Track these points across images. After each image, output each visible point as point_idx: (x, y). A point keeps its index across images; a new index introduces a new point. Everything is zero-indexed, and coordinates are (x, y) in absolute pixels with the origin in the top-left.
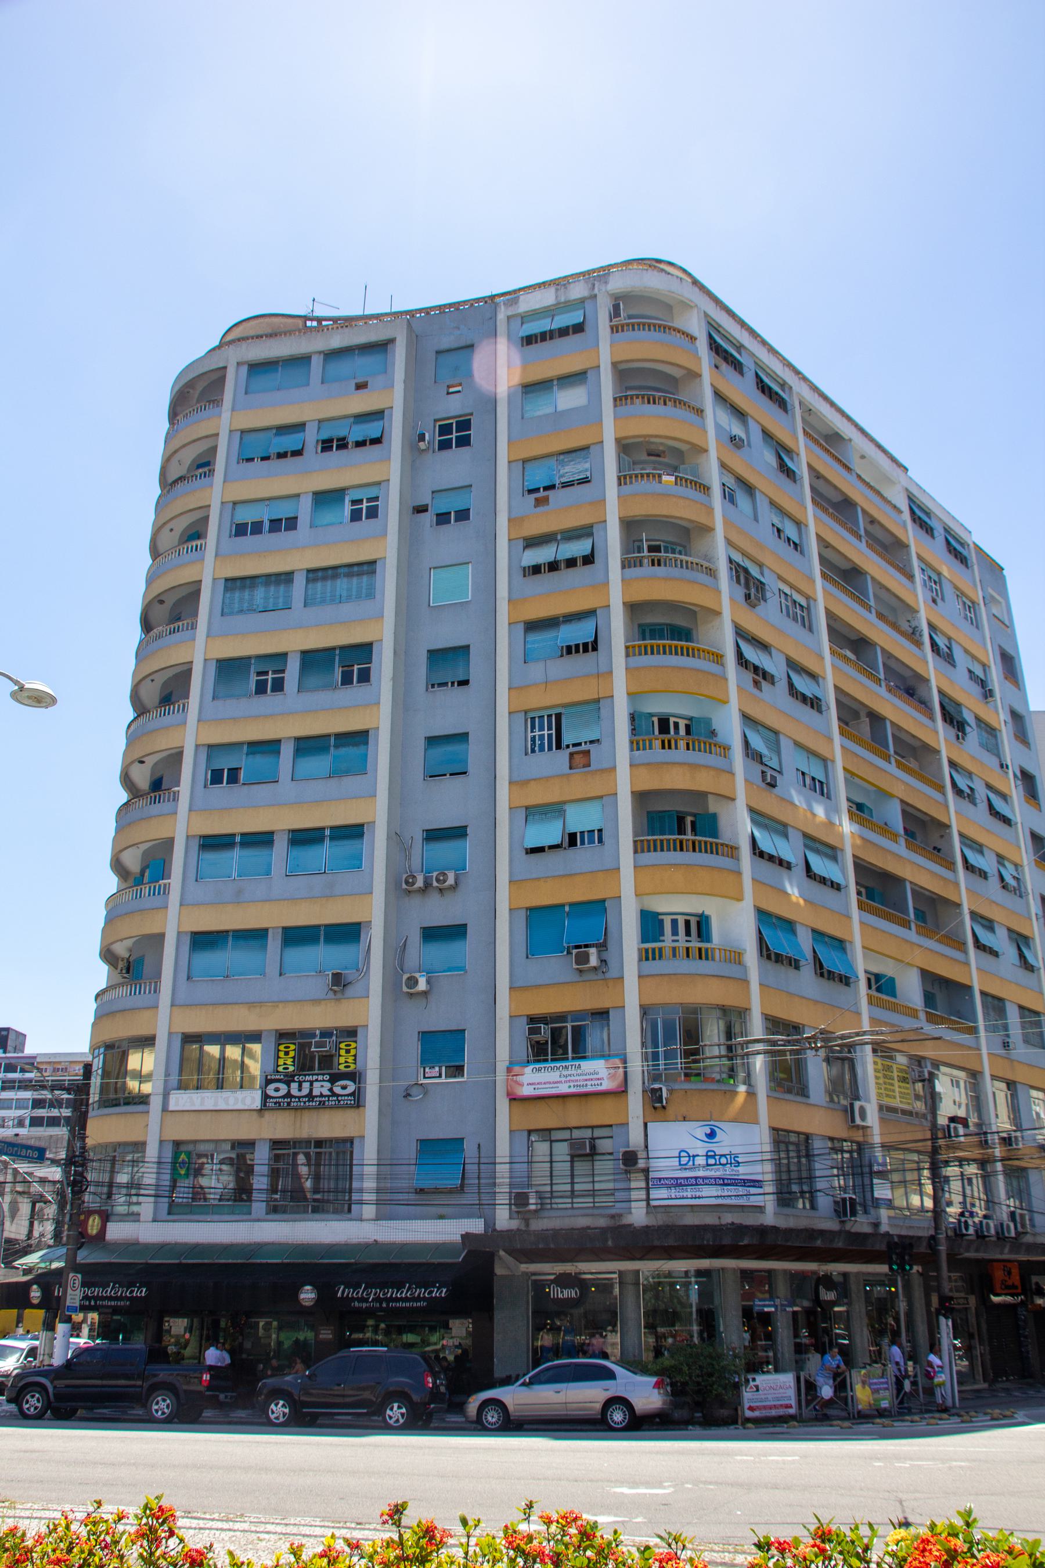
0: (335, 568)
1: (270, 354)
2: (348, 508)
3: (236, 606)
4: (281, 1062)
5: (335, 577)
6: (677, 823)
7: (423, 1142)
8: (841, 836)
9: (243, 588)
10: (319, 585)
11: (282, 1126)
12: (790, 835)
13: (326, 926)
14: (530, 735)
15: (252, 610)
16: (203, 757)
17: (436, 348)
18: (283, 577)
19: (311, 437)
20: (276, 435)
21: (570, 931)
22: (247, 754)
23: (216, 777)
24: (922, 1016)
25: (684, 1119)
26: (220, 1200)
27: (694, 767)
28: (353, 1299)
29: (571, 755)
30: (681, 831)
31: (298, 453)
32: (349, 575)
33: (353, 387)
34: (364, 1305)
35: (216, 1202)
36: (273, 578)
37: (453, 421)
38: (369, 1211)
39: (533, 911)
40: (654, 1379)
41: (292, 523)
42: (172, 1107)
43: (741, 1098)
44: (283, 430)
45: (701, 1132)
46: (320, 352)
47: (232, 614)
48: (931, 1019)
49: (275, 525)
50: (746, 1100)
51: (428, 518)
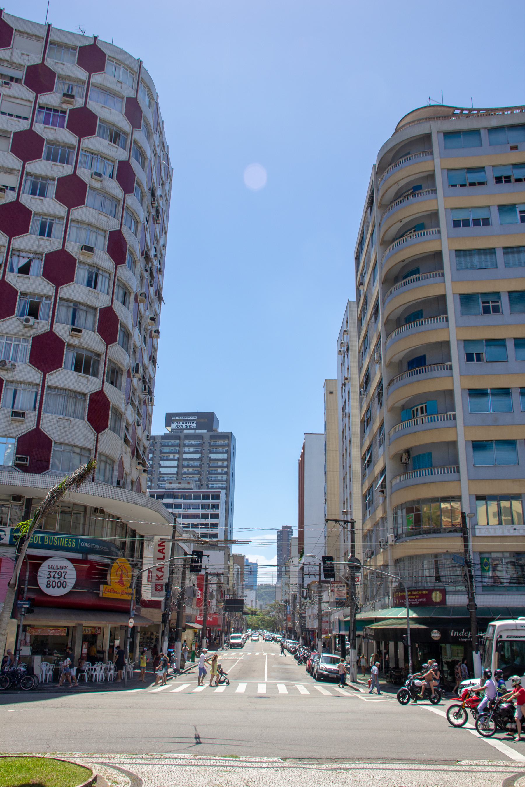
3: (463, 265)
5: (519, 252)
9: (465, 256)
15: (473, 268)
18: (488, 251)
19: (489, 176)
22: (486, 346)
23: (470, 358)
26: (510, 583)
28: (459, 637)
29: (90, 450)
31: (481, 183)
35: (508, 585)
36: (482, 251)
41: (486, 222)
44: (471, 170)
46: (485, 128)
47: (461, 269)
49: (476, 222)
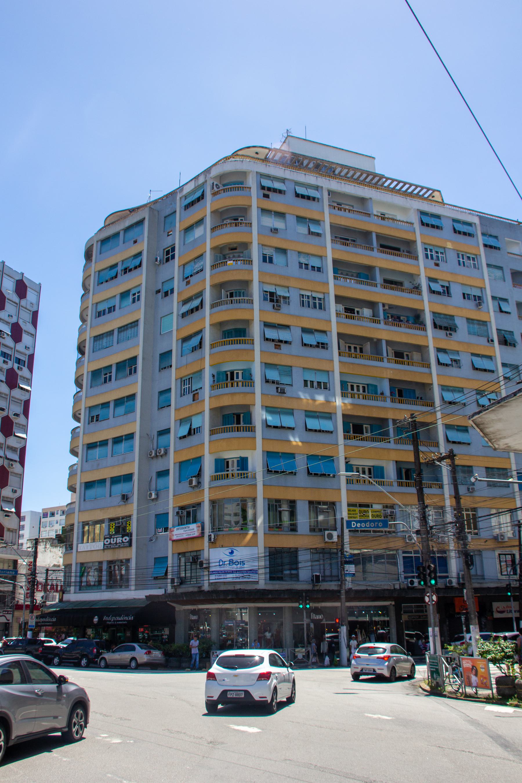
0: (103, 334)
1: (121, 229)
2: (131, 297)
4: (111, 530)
5: (127, 329)
6: (234, 419)
7: (155, 559)
8: (335, 407)
10: (122, 333)
11: (109, 556)
12: (294, 414)
13: (123, 475)
14: (183, 388)
16: (87, 412)
17: (164, 215)
20: (110, 270)
21: (191, 470)
24: (395, 484)
25: (222, 547)
27: (233, 394)
30: (238, 422)
32: (131, 327)
33: (132, 242)
34: (110, 623)
37: (170, 248)
38: (133, 588)
39: (181, 463)
40: (146, 651)
42: (79, 551)
43: (249, 537)
45: (227, 551)
47: (96, 351)
48: (400, 484)
50: (251, 538)
51: (160, 295)
